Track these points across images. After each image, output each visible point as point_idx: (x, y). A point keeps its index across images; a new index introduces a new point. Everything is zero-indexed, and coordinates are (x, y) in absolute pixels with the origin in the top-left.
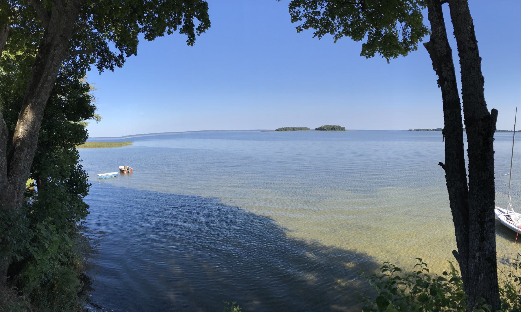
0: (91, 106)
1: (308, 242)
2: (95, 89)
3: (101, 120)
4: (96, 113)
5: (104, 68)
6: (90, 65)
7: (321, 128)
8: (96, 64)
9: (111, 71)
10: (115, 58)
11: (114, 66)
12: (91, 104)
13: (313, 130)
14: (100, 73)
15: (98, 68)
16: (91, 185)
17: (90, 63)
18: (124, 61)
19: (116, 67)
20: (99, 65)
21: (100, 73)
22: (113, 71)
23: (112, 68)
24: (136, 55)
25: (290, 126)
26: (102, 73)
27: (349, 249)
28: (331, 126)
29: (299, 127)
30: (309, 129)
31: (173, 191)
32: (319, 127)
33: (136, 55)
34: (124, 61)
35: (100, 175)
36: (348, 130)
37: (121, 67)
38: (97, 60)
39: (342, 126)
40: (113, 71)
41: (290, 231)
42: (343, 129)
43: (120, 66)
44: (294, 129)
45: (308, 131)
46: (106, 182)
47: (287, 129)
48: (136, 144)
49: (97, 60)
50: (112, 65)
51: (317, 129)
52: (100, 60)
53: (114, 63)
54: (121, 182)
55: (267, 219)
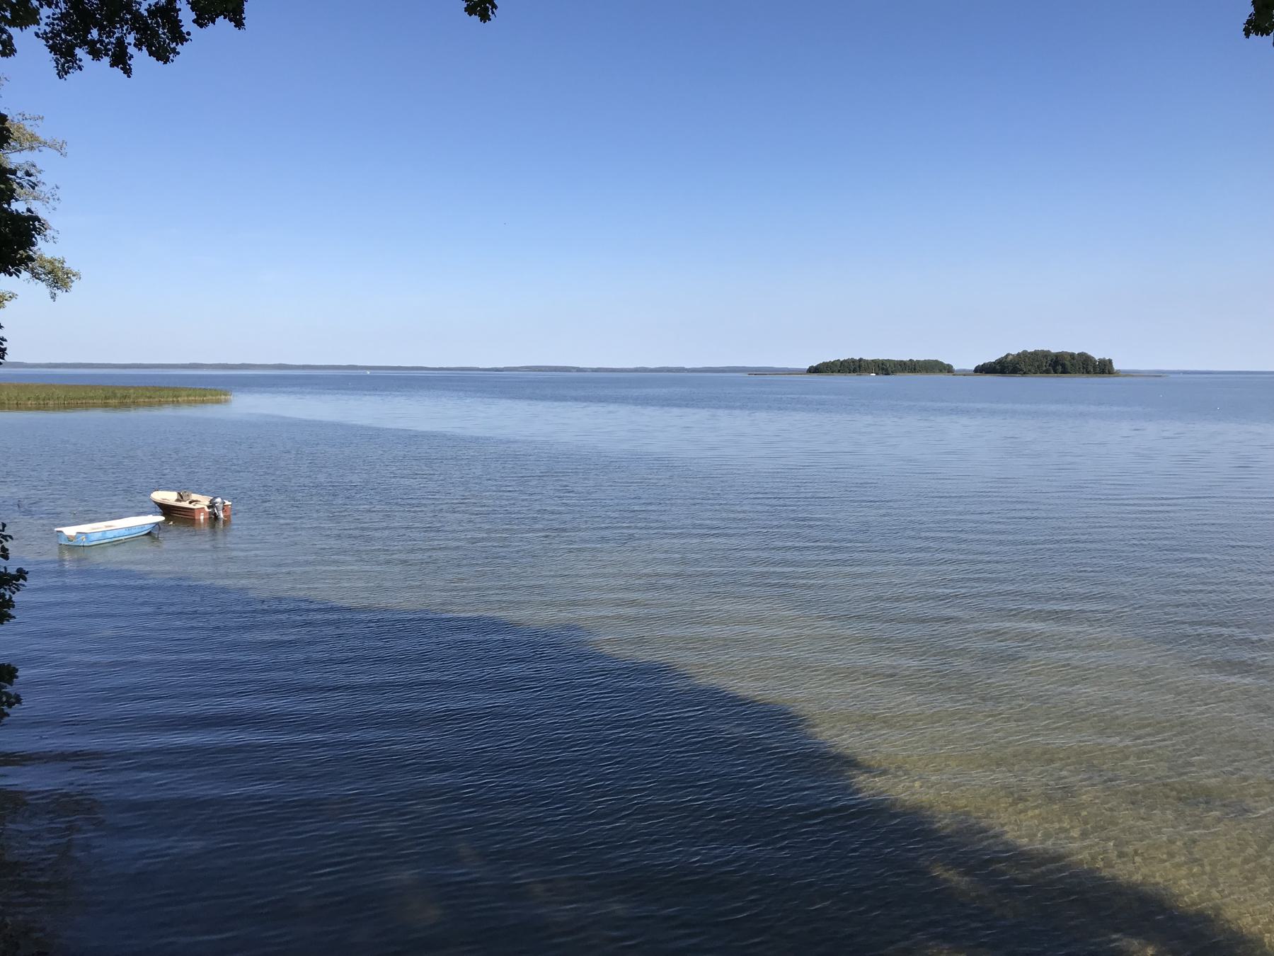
0: (17, 217)
1: (944, 823)
2: (34, 143)
3: (76, 285)
4: (43, 248)
5: (80, 52)
6: (14, 31)
7: (1000, 362)
8: (43, 27)
9: (118, 71)
10: (137, 16)
11: (131, 50)
12: (18, 206)
13: (965, 373)
14: (63, 72)
15: (53, 48)
16: (21, 574)
17: (12, 23)
18: (180, 37)
19: (140, 58)
20: (56, 35)
21: (63, 72)
22: (127, 71)
23: (121, 60)
24: (239, 24)
25: (869, 356)
26: (74, 76)
27: (1138, 877)
28: (1046, 354)
29: (905, 358)
30: (948, 369)
31: (404, 600)
32: (992, 358)
33: (239, 24)
34: (180, 37)
35: (70, 531)
36: (1128, 374)
37: (166, 60)
38: (45, 12)
39: (1097, 354)
40: (127, 71)
41: (868, 770)
42: (1104, 368)
43: (162, 54)
44: (884, 368)
45: (949, 377)
46: (97, 557)
47: (855, 367)
48: (245, 405)
49: (45, 12)
50: (121, 44)
51: (984, 370)
52: (63, 17)
53: (131, 39)
54: (185, 558)
55: (781, 719)
